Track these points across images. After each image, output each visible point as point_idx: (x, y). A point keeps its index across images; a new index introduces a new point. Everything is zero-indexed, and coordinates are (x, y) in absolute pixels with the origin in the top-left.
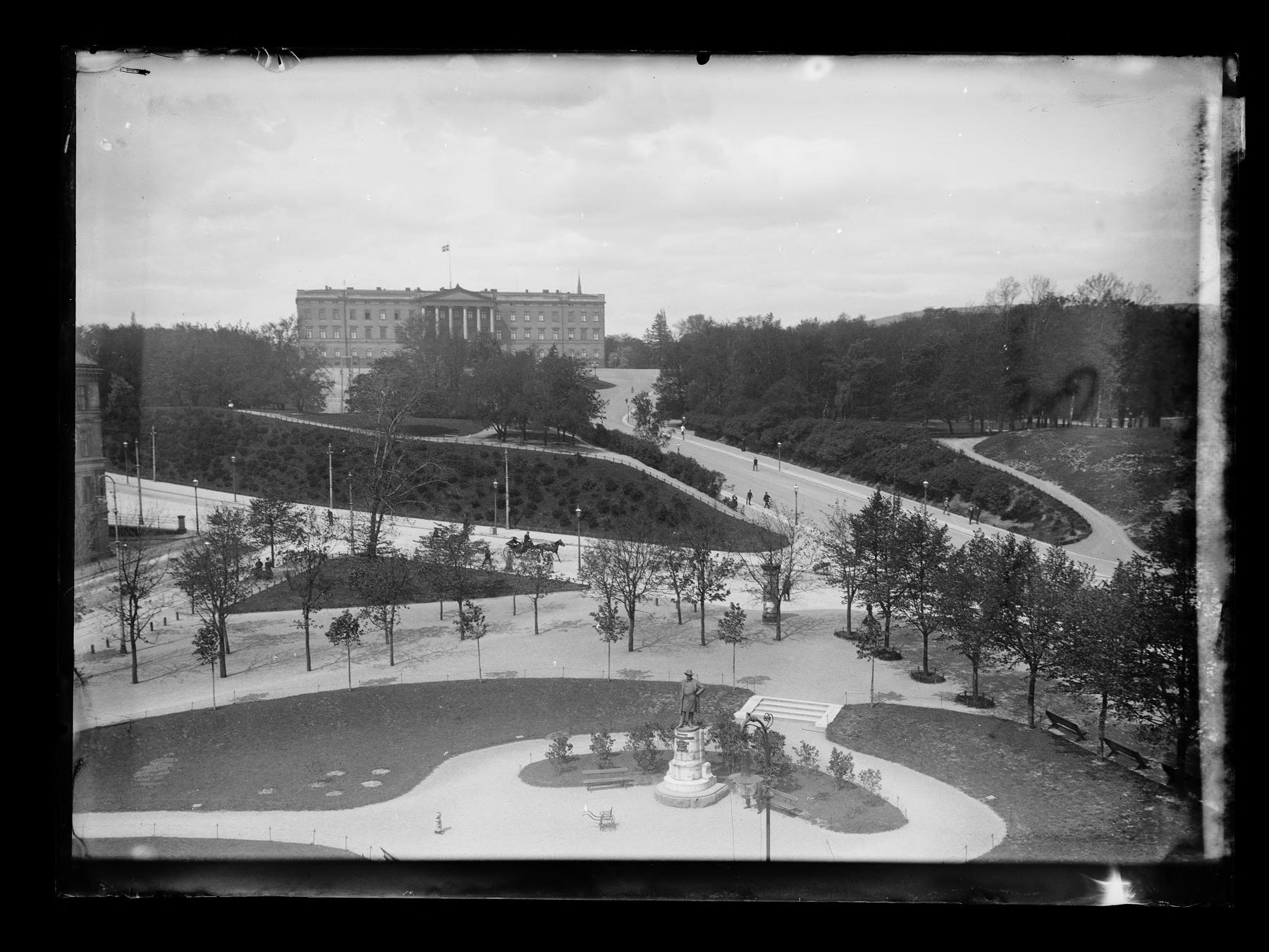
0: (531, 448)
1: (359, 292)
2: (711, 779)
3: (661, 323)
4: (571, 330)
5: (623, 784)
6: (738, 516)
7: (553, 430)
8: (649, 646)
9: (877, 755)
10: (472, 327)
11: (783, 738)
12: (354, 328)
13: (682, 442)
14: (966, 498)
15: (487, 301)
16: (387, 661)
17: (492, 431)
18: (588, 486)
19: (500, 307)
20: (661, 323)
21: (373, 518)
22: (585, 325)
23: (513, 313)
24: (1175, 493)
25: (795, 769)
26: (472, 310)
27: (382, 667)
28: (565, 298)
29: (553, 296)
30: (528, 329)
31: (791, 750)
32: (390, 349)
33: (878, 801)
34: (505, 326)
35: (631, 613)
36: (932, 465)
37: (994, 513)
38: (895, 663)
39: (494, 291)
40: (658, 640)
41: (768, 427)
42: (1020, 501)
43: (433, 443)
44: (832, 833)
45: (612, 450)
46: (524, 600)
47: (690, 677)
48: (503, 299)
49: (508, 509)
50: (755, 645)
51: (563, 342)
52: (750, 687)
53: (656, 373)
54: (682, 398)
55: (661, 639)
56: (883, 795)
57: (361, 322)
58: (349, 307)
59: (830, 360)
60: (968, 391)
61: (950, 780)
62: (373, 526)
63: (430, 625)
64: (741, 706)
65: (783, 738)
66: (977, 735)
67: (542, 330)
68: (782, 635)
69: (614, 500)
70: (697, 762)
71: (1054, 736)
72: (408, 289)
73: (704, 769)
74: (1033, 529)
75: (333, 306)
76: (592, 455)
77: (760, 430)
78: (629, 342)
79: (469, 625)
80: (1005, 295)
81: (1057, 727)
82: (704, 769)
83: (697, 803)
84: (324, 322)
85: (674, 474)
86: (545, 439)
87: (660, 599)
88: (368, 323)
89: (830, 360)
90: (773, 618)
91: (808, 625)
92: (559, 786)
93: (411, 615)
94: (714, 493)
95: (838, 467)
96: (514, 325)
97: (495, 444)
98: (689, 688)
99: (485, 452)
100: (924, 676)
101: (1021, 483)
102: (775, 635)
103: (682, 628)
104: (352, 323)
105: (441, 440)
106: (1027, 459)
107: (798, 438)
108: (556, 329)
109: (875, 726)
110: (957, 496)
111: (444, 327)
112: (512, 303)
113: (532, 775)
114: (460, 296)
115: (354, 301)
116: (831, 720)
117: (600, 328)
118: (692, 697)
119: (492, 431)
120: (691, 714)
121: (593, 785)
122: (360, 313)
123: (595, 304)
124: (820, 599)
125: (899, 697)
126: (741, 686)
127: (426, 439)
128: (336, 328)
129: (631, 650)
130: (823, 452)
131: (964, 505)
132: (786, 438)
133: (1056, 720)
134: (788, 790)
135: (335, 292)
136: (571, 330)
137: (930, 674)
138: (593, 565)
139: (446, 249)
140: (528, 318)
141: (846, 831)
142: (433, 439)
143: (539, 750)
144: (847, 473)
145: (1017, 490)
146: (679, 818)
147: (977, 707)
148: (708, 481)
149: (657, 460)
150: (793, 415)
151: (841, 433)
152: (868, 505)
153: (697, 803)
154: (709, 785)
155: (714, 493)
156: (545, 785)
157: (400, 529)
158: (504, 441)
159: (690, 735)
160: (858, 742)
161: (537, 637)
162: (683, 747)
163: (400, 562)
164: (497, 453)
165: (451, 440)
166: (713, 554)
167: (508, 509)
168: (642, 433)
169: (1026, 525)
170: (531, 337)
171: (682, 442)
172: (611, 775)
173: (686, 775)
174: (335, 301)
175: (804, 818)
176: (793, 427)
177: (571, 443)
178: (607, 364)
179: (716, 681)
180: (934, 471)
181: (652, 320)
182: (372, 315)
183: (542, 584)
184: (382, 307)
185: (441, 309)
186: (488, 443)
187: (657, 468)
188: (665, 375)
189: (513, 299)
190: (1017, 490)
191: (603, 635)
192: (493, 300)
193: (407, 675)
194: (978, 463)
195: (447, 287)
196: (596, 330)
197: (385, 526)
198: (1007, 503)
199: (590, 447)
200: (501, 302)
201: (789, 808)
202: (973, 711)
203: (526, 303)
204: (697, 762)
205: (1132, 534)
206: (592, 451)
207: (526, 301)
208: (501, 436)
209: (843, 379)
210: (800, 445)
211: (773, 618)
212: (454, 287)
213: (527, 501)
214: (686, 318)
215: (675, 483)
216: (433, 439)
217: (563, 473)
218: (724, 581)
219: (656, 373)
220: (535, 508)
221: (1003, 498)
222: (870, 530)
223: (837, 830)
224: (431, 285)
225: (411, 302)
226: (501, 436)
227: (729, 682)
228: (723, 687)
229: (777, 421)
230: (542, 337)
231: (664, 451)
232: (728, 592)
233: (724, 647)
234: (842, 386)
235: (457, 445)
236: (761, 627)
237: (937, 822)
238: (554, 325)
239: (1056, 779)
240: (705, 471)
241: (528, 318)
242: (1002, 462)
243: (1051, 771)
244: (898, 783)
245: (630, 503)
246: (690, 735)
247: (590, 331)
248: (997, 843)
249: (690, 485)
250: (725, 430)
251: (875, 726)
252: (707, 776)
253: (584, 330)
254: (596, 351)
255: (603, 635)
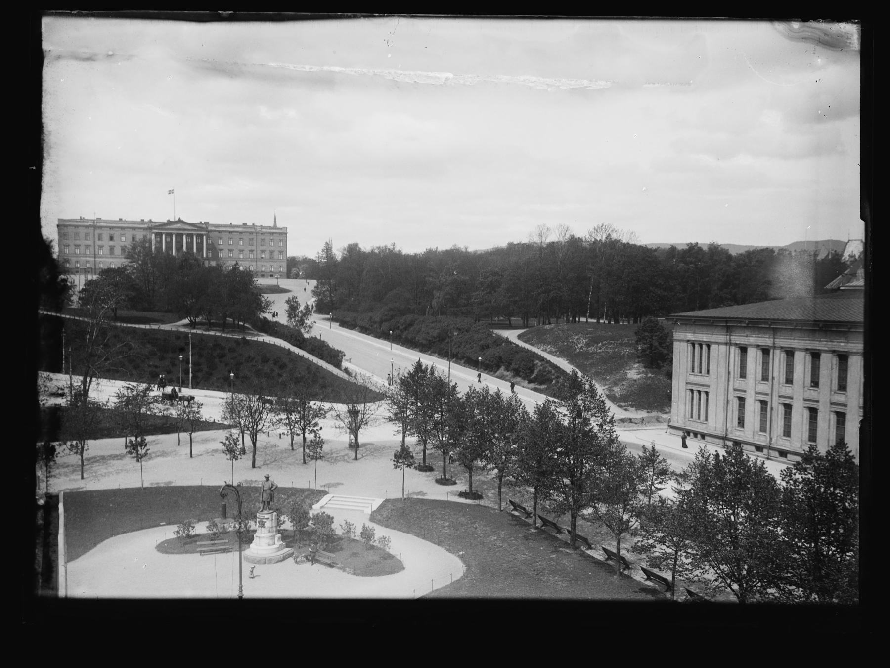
0: (212, 333)
1: (105, 221)
2: (281, 545)
3: (328, 249)
4: (263, 251)
5: (225, 551)
6: (352, 380)
7: (230, 320)
8: (267, 464)
9: (399, 530)
10: (179, 247)
11: (333, 518)
12: (101, 247)
13: (322, 328)
14: (507, 369)
15: (202, 230)
16: (80, 477)
17: (186, 321)
18: (250, 359)
19: (211, 234)
20: (328, 249)
21: (85, 380)
22: (272, 249)
23: (221, 238)
24: (636, 366)
25: (340, 539)
26: (190, 236)
27: (75, 480)
28: (258, 229)
29: (250, 227)
30: (231, 251)
31: (338, 528)
32: (116, 262)
33: (390, 557)
34: (215, 248)
35: (254, 443)
36: (488, 347)
37: (524, 379)
38: (428, 473)
39: (207, 223)
40: (275, 460)
41: (386, 321)
42: (540, 371)
43: (142, 329)
44: (355, 576)
45: (271, 335)
46: (184, 436)
47: (267, 479)
48: (213, 229)
49: (191, 375)
50: (340, 464)
51: (244, 260)
52: (327, 489)
53: (314, 283)
54: (332, 301)
55: (276, 459)
56: (392, 552)
57: (106, 242)
58: (98, 232)
59: (430, 276)
60: (517, 298)
61: (439, 543)
62: (85, 387)
63: (118, 453)
64: (318, 501)
65: (333, 518)
66: (464, 516)
67: (241, 251)
68: (359, 456)
69: (266, 369)
70: (271, 534)
71: (513, 516)
72: (143, 220)
73: (276, 539)
74: (547, 389)
75: (85, 231)
76: (255, 339)
77: (381, 322)
78: (306, 261)
79: (137, 451)
80: (541, 236)
81: (517, 510)
82: (276, 539)
83: (270, 561)
84: (78, 242)
85: (311, 351)
86: (224, 327)
87: (275, 430)
88: (111, 243)
89: (430, 276)
90: (355, 446)
91: (376, 450)
92: (182, 553)
93: (95, 447)
94: (338, 365)
95: (430, 348)
96: (221, 247)
97: (187, 330)
98: (267, 486)
99: (178, 335)
100: (443, 481)
101: (542, 359)
102: (353, 457)
103: (294, 453)
104: (100, 243)
105: (148, 327)
106: (549, 343)
107: (406, 329)
108: (251, 251)
109: (405, 514)
110: (502, 368)
111: (159, 248)
112: (219, 232)
113: (165, 548)
114: (179, 226)
115: (101, 227)
116: (375, 508)
117: (283, 251)
118: (269, 492)
119: (186, 321)
120: (268, 503)
121: (204, 552)
122: (106, 237)
123: (280, 234)
124: (382, 430)
125: (424, 494)
126: (322, 489)
127: (137, 326)
128: (87, 247)
129: (254, 466)
130: (420, 338)
131: (506, 373)
132: (398, 328)
133: (516, 507)
134: (330, 551)
135: (87, 221)
136: (263, 251)
137: (448, 480)
138: (232, 411)
139: (171, 192)
140: (231, 242)
141: (363, 575)
142: (142, 326)
143: (168, 532)
144: (435, 352)
145: (540, 364)
146: (268, 571)
147: (471, 499)
148: (334, 357)
149: (300, 342)
150: (402, 313)
151: (433, 325)
152: (412, 370)
153: (270, 561)
154: (279, 549)
155: (338, 365)
156: (172, 553)
157: (103, 388)
158: (194, 328)
159: (266, 516)
160: (386, 523)
161: (192, 460)
162: (262, 525)
163: (97, 408)
164: (186, 335)
165: (155, 327)
166: (312, 404)
167: (191, 375)
168: (293, 323)
169: (543, 387)
170: (232, 256)
171: (322, 328)
172: (222, 544)
173: (265, 543)
174: (87, 227)
175: (339, 568)
176: (402, 321)
177: (243, 329)
178: (289, 276)
179: (305, 486)
180: (488, 352)
181: (322, 246)
182: (115, 238)
183: (197, 425)
184: (123, 232)
185: (167, 235)
186: (182, 330)
187: (300, 348)
188: (321, 283)
189: (220, 229)
190: (540, 364)
191: (229, 457)
192: (206, 230)
193: (92, 485)
194: (517, 346)
195: (172, 219)
196: (281, 252)
197: (93, 385)
198: (532, 372)
199: (256, 333)
200: (211, 231)
201: (329, 561)
202: (469, 502)
203: (230, 232)
204: (271, 534)
205: (607, 393)
206: (257, 335)
207: (231, 232)
208: (192, 325)
209: (439, 289)
210: (406, 333)
211: (355, 446)
212: (177, 219)
213: (205, 368)
214: (346, 245)
215: (311, 357)
216: (142, 326)
217: (232, 350)
218: (317, 420)
219: (314, 283)
220: (211, 374)
221: (529, 369)
222: (420, 389)
223: (357, 574)
224: (160, 217)
225: (144, 229)
226: (192, 325)
227: (313, 486)
228: (308, 490)
229: (392, 317)
230: (241, 256)
231: (306, 336)
232: (321, 428)
233: (243, 456)
234: (437, 294)
235: (159, 330)
236: (347, 452)
237: (423, 570)
238: (250, 248)
239: (504, 541)
240: (333, 350)
241: (231, 242)
242: (533, 345)
243: (502, 536)
244: (400, 543)
245: (277, 371)
246: (266, 516)
247: (276, 253)
248: (455, 579)
249: (322, 359)
250: (359, 323)
251: (405, 514)
252: (278, 543)
253: (272, 252)
254: (280, 266)
255: (229, 457)
